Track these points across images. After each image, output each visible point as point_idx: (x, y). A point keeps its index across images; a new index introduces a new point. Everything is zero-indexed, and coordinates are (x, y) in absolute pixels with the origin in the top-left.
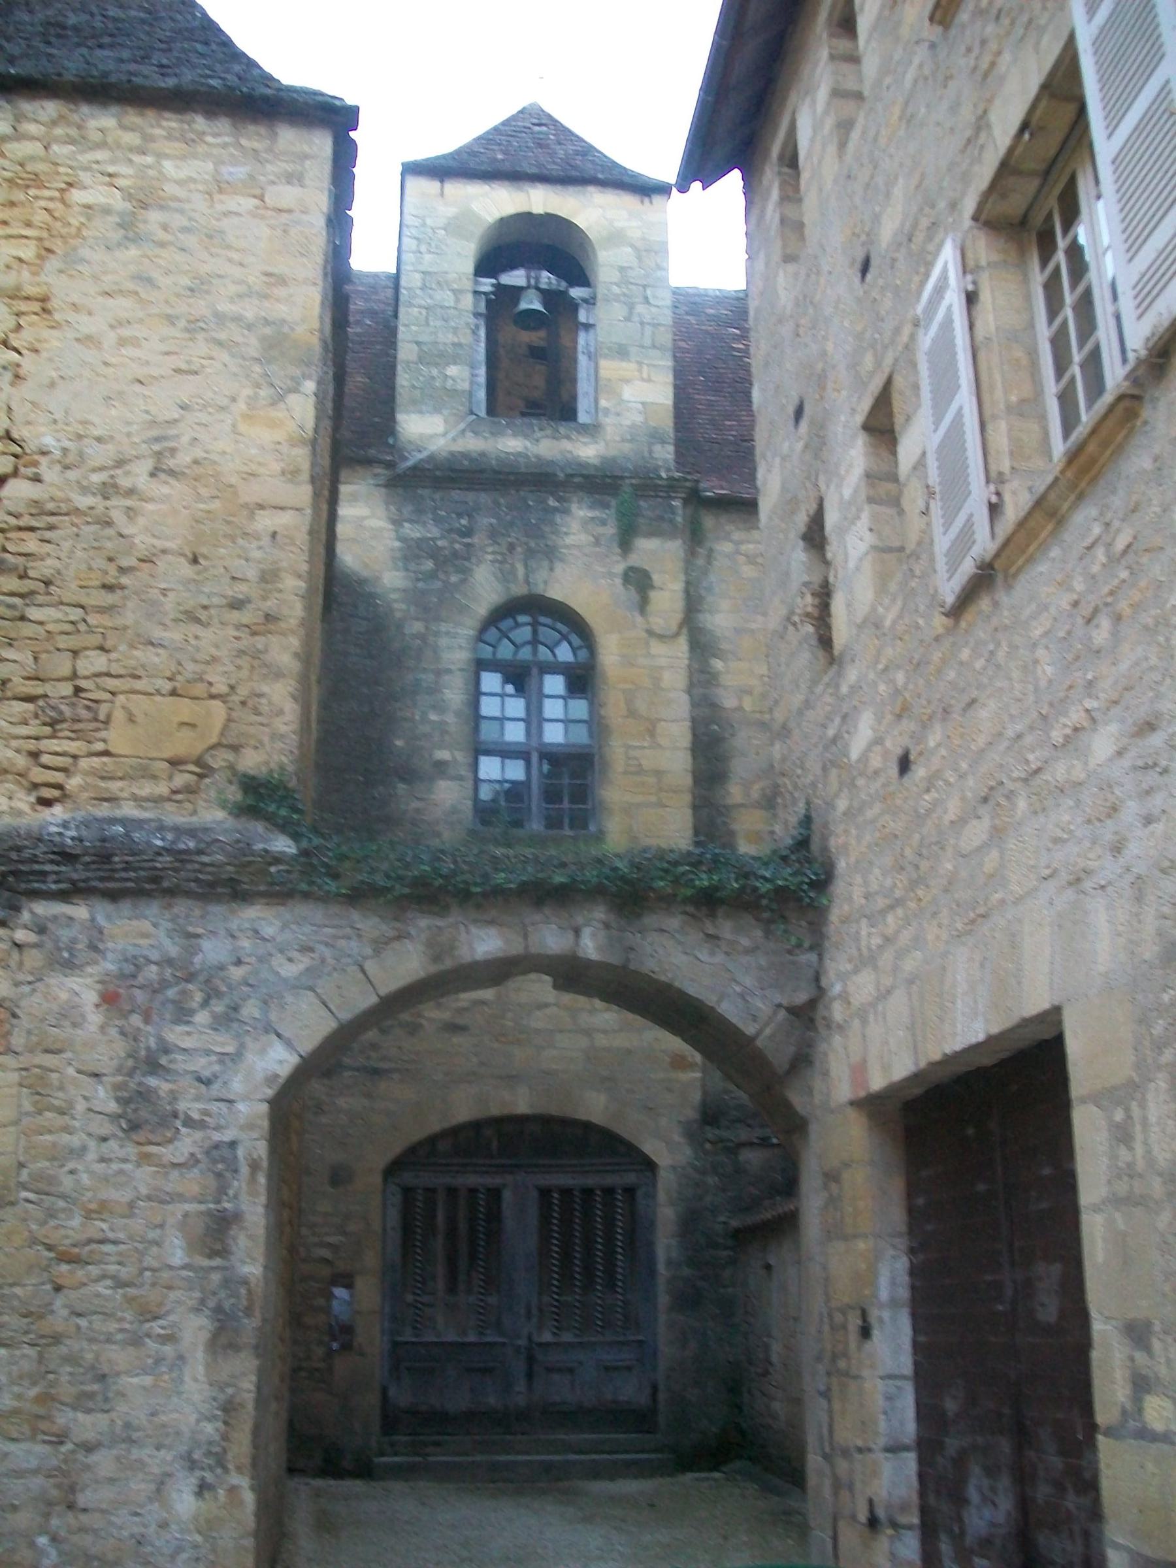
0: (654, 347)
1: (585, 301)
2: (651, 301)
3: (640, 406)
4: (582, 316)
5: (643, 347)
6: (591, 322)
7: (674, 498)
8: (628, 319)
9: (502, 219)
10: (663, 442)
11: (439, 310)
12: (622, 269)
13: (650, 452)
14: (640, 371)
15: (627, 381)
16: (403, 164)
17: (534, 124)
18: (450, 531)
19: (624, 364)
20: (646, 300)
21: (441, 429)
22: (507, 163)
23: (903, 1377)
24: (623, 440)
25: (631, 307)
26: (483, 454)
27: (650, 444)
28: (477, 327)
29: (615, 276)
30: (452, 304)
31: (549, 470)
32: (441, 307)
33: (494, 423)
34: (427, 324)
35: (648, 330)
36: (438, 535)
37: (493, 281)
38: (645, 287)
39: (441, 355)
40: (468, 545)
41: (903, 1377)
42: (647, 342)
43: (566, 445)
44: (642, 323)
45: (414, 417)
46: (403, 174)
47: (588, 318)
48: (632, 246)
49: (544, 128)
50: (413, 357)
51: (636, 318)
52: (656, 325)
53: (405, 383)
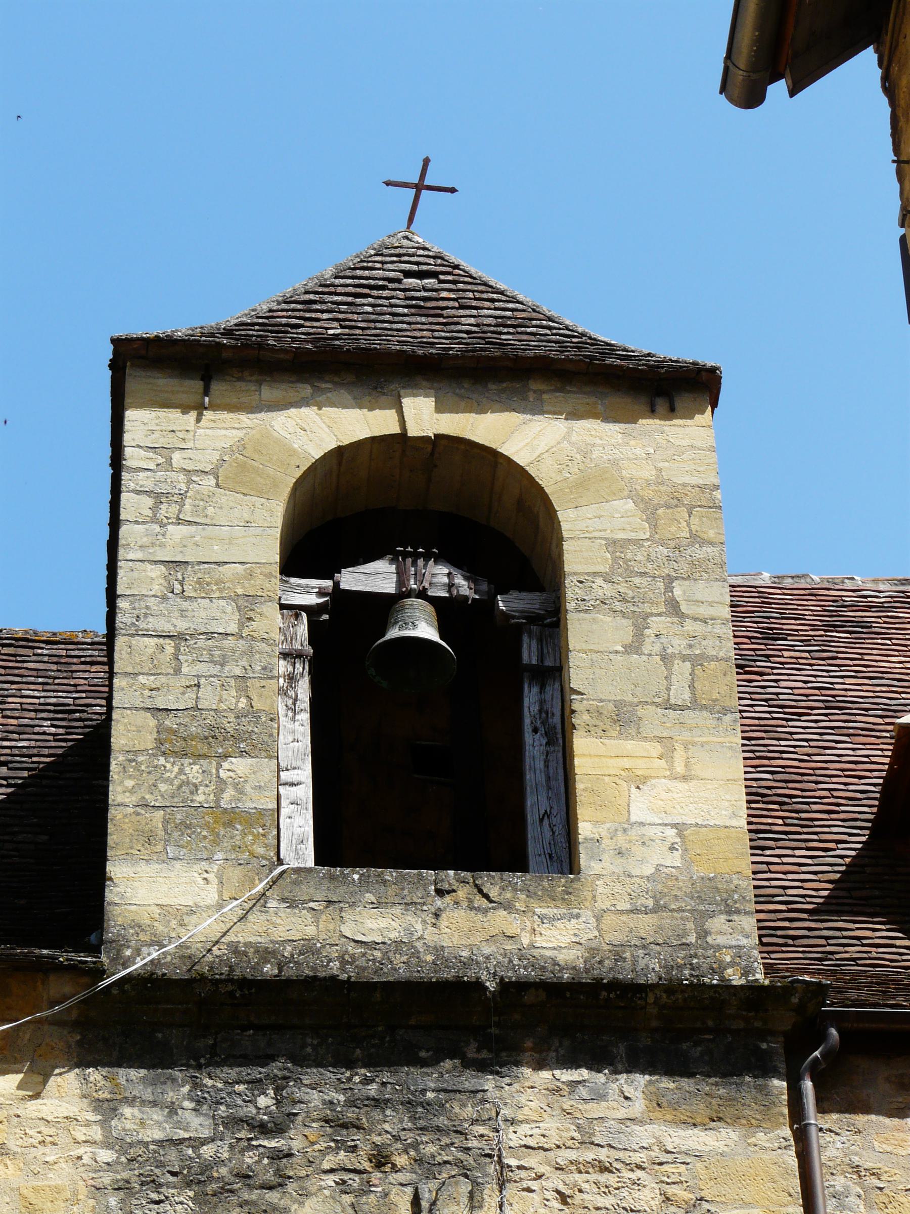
0: (695, 704)
1: (533, 618)
2: (684, 608)
3: (671, 832)
4: (529, 653)
5: (668, 706)
6: (549, 663)
7: (763, 1035)
8: (634, 647)
9: (339, 452)
10: (730, 911)
11: (202, 642)
12: (613, 544)
13: (704, 933)
14: (667, 755)
15: (640, 782)
16: (117, 342)
17: (408, 274)
18: (235, 1122)
19: (630, 745)
20: (674, 607)
21: (211, 895)
22: (514, 978)
23: (112, 805)
24: (634, 911)
25: (640, 623)
26: (309, 947)
27: (701, 917)
28: (291, 679)
29: (602, 562)
30: (233, 628)
31: (469, 975)
32: (209, 635)
33: (332, 878)
34: (178, 671)
35: (683, 669)
36: (206, 1133)
37: (328, 583)
38: (669, 581)
39: (214, 735)
40: (278, 1156)
41: (112, 805)
42: (680, 694)
43: (500, 920)
44: (666, 658)
45: (144, 869)
46: (117, 366)
47: (541, 657)
48: (635, 496)
49: (430, 282)
50: (148, 741)
51: (650, 646)
52: (698, 661)
53: (128, 799)
